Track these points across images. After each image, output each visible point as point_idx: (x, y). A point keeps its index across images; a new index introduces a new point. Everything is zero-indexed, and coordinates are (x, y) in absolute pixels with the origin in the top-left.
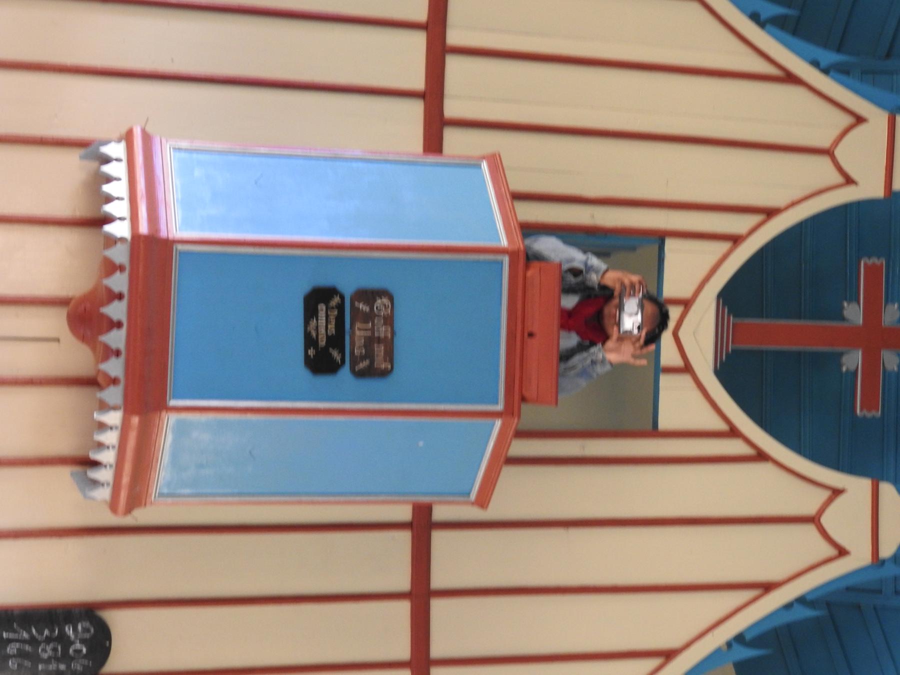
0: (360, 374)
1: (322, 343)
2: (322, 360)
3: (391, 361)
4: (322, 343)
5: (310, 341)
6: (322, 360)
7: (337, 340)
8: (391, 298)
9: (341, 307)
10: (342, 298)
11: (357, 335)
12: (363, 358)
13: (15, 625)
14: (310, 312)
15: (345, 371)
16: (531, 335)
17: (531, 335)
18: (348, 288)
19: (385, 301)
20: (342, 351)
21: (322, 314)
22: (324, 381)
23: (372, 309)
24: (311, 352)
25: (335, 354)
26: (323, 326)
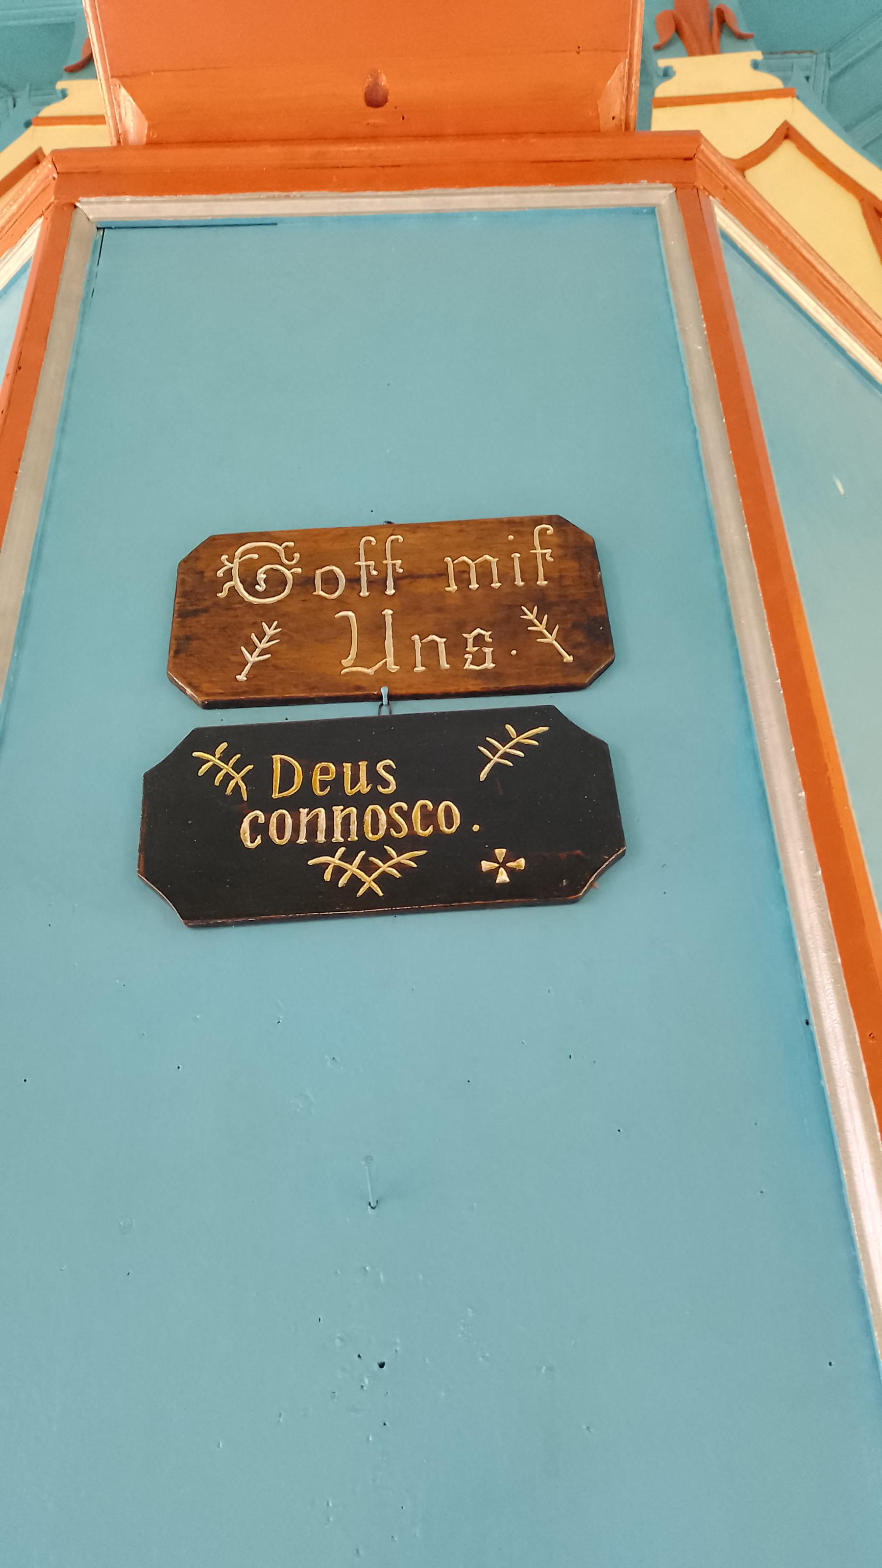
0: (594, 643)
1: (449, 816)
2: (536, 824)
3: (521, 526)
4: (449, 816)
5: (441, 883)
6: (536, 824)
7: (430, 754)
8: (219, 545)
9: (251, 745)
10: (202, 739)
11: (389, 666)
12: (510, 630)
13: (299, 570)
14: (287, 890)
15: (579, 708)
16: (375, 100)
17: (375, 100)
18: (171, 717)
19: (231, 564)
20: (493, 723)
21: (285, 828)
22: (644, 793)
23: (268, 613)
24: (500, 867)
25: (498, 754)
26: (376, 818)
